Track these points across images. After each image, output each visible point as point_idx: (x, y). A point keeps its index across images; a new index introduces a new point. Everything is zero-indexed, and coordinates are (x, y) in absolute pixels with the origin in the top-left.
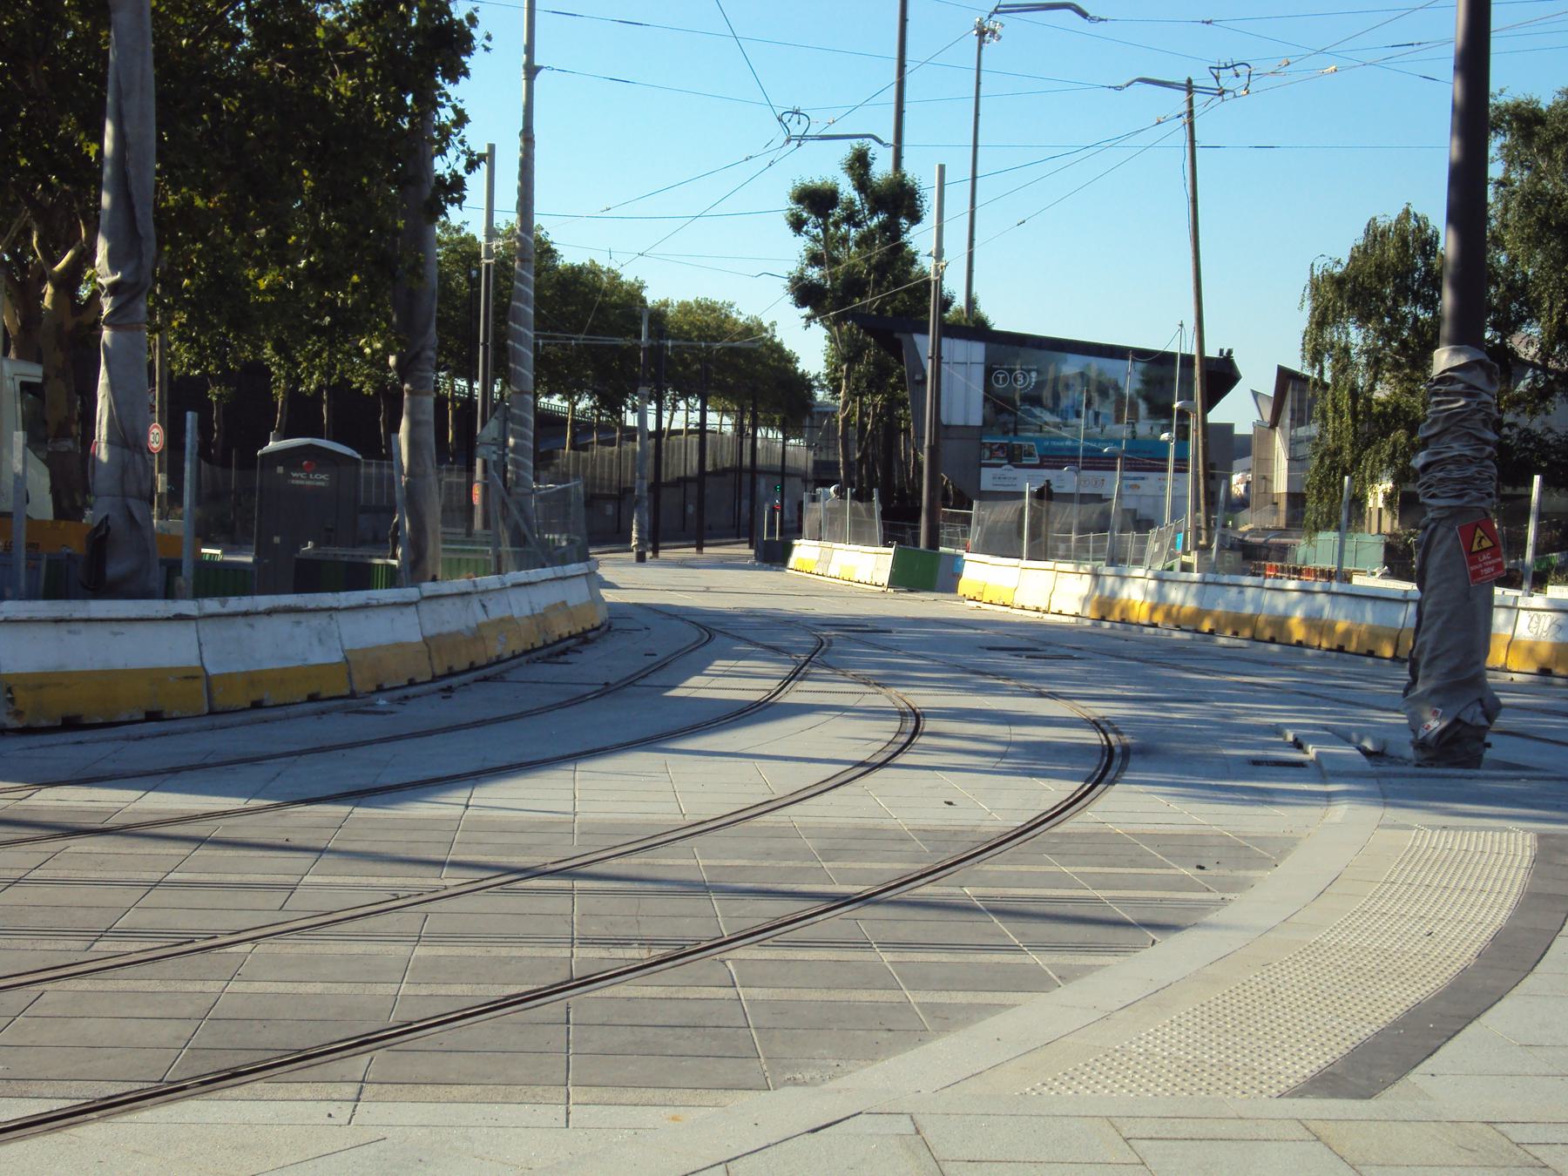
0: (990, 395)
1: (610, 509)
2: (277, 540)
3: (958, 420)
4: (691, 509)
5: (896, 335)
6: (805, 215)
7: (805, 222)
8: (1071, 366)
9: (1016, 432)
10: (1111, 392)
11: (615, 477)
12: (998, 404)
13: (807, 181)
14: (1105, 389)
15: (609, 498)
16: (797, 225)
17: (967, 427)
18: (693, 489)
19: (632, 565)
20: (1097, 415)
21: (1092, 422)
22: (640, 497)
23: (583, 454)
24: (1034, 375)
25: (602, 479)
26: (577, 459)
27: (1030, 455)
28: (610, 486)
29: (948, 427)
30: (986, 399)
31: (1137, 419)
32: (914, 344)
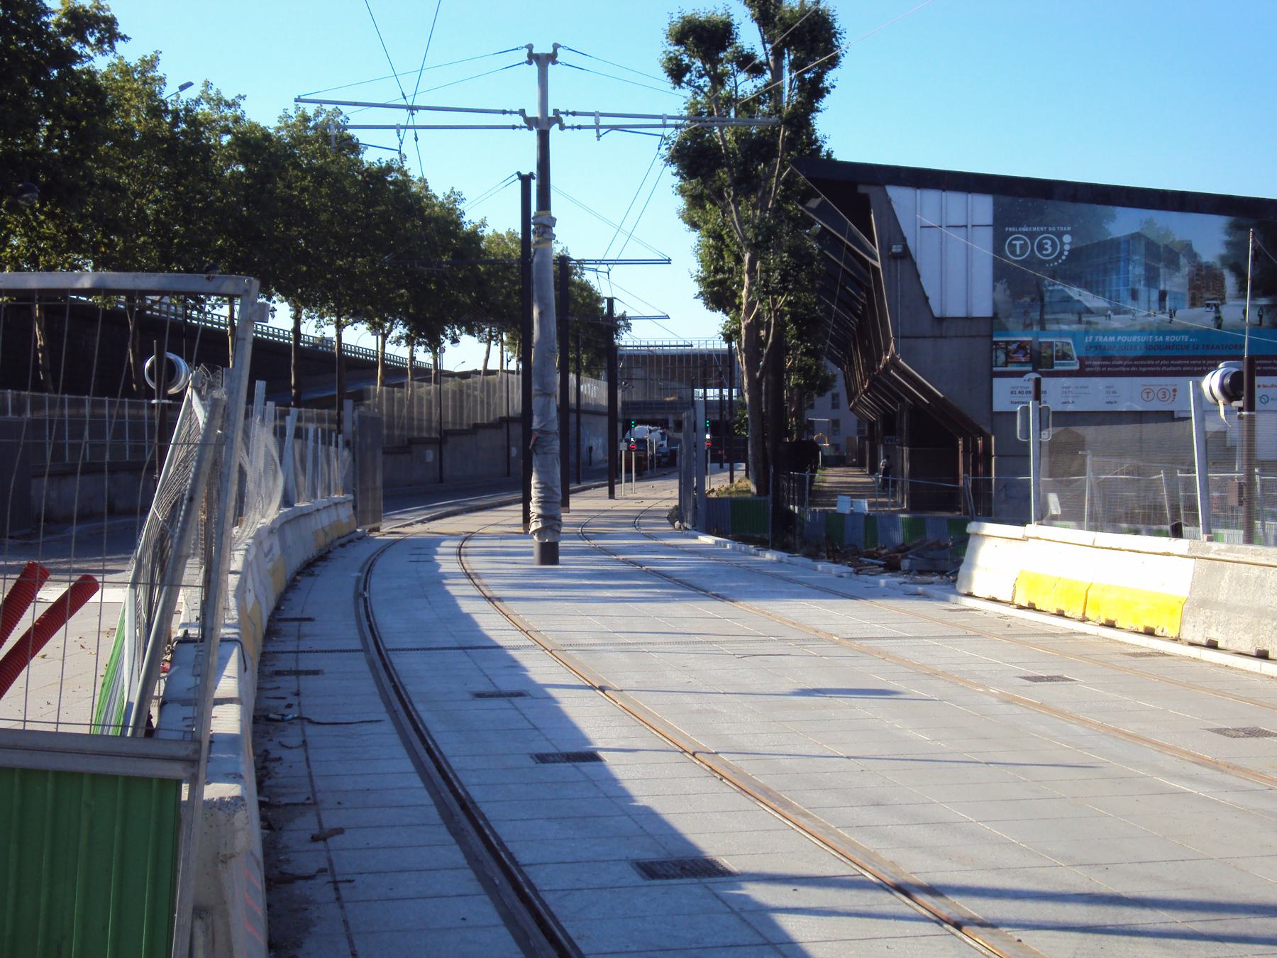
0: (1001, 272)
1: (430, 455)
2: (708, 436)
3: (955, 309)
4: (514, 452)
5: (862, 189)
6: (686, 60)
7: (688, 68)
8: (1124, 223)
9: (1042, 324)
10: (1183, 260)
11: (435, 417)
12: (1014, 279)
13: (688, 12)
14: (1162, 256)
15: (427, 442)
16: (677, 72)
17: (969, 319)
18: (517, 430)
19: (1167, 535)
20: (1163, 296)
21: (1155, 306)
22: (543, 432)
23: (397, 393)
24: (1067, 239)
25: (420, 420)
26: (391, 399)
27: (1065, 356)
28: (429, 429)
29: (941, 320)
30: (997, 278)
31: (1223, 300)
32: (889, 201)
